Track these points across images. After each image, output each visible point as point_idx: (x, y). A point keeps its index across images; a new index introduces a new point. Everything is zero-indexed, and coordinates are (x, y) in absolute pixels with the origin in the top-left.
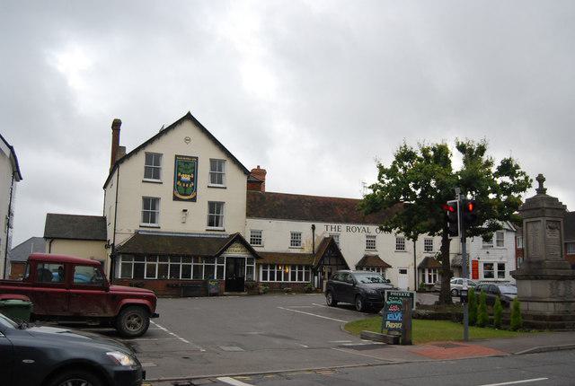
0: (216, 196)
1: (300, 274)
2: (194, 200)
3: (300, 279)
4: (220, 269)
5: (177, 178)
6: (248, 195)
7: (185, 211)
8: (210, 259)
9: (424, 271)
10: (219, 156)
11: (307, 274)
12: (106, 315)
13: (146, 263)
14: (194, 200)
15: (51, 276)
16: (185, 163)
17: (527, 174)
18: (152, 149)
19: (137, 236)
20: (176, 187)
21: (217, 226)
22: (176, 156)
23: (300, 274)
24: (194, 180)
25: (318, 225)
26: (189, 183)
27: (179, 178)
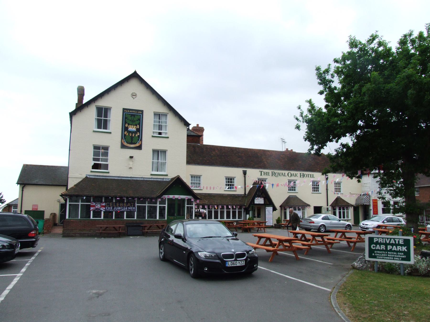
0: (160, 144)
1: (234, 213)
3: (234, 217)
4: (162, 209)
5: (125, 129)
7: (131, 157)
8: (153, 200)
10: (162, 109)
11: (240, 213)
12: (272, 171)
17: (203, 190)
18: (102, 103)
19: (87, 180)
20: (124, 137)
23: (234, 213)
24: (139, 130)
25: (250, 171)
26: (135, 133)
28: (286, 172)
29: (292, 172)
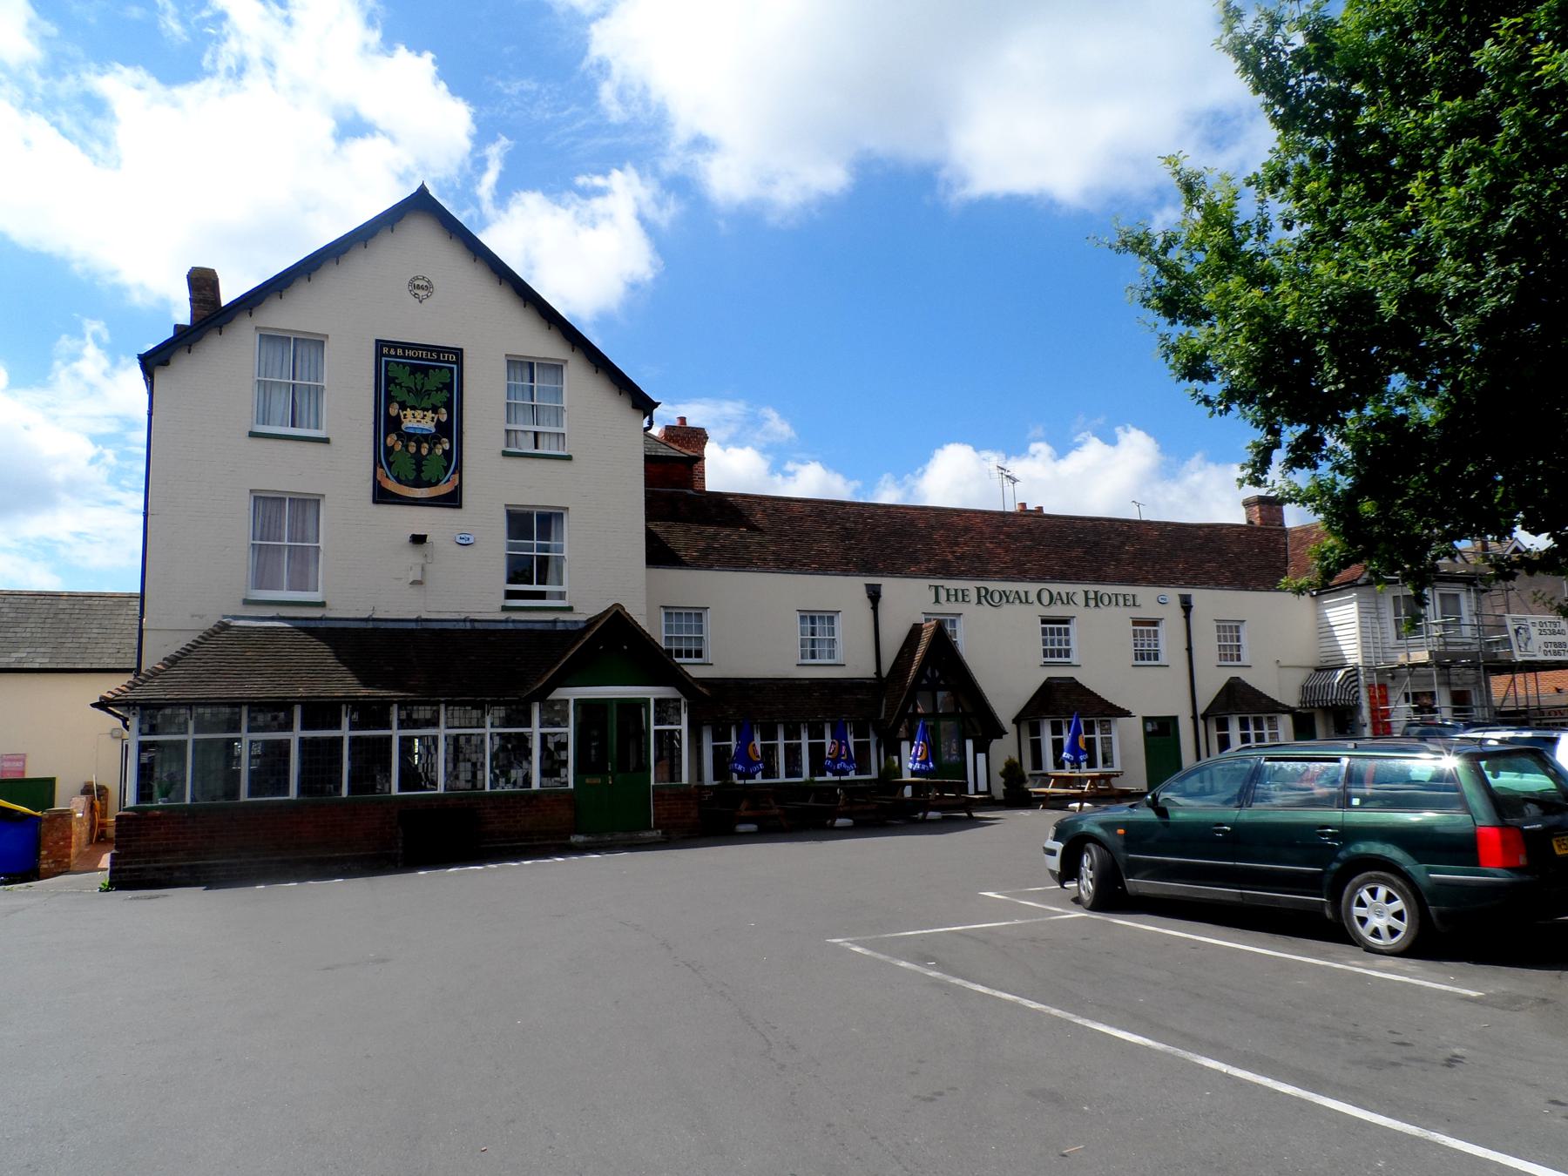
2: (453, 500)
5: (387, 424)
6: (646, 492)
7: (418, 540)
9: (1035, 730)
13: (396, 734)
14: (453, 500)
15: (1343, 411)
16: (415, 369)
20: (383, 457)
21: (542, 581)
22: (380, 344)
24: (450, 429)
25: (891, 587)
26: (432, 439)
27: (393, 424)
28: (1033, 588)
29: (1056, 588)
